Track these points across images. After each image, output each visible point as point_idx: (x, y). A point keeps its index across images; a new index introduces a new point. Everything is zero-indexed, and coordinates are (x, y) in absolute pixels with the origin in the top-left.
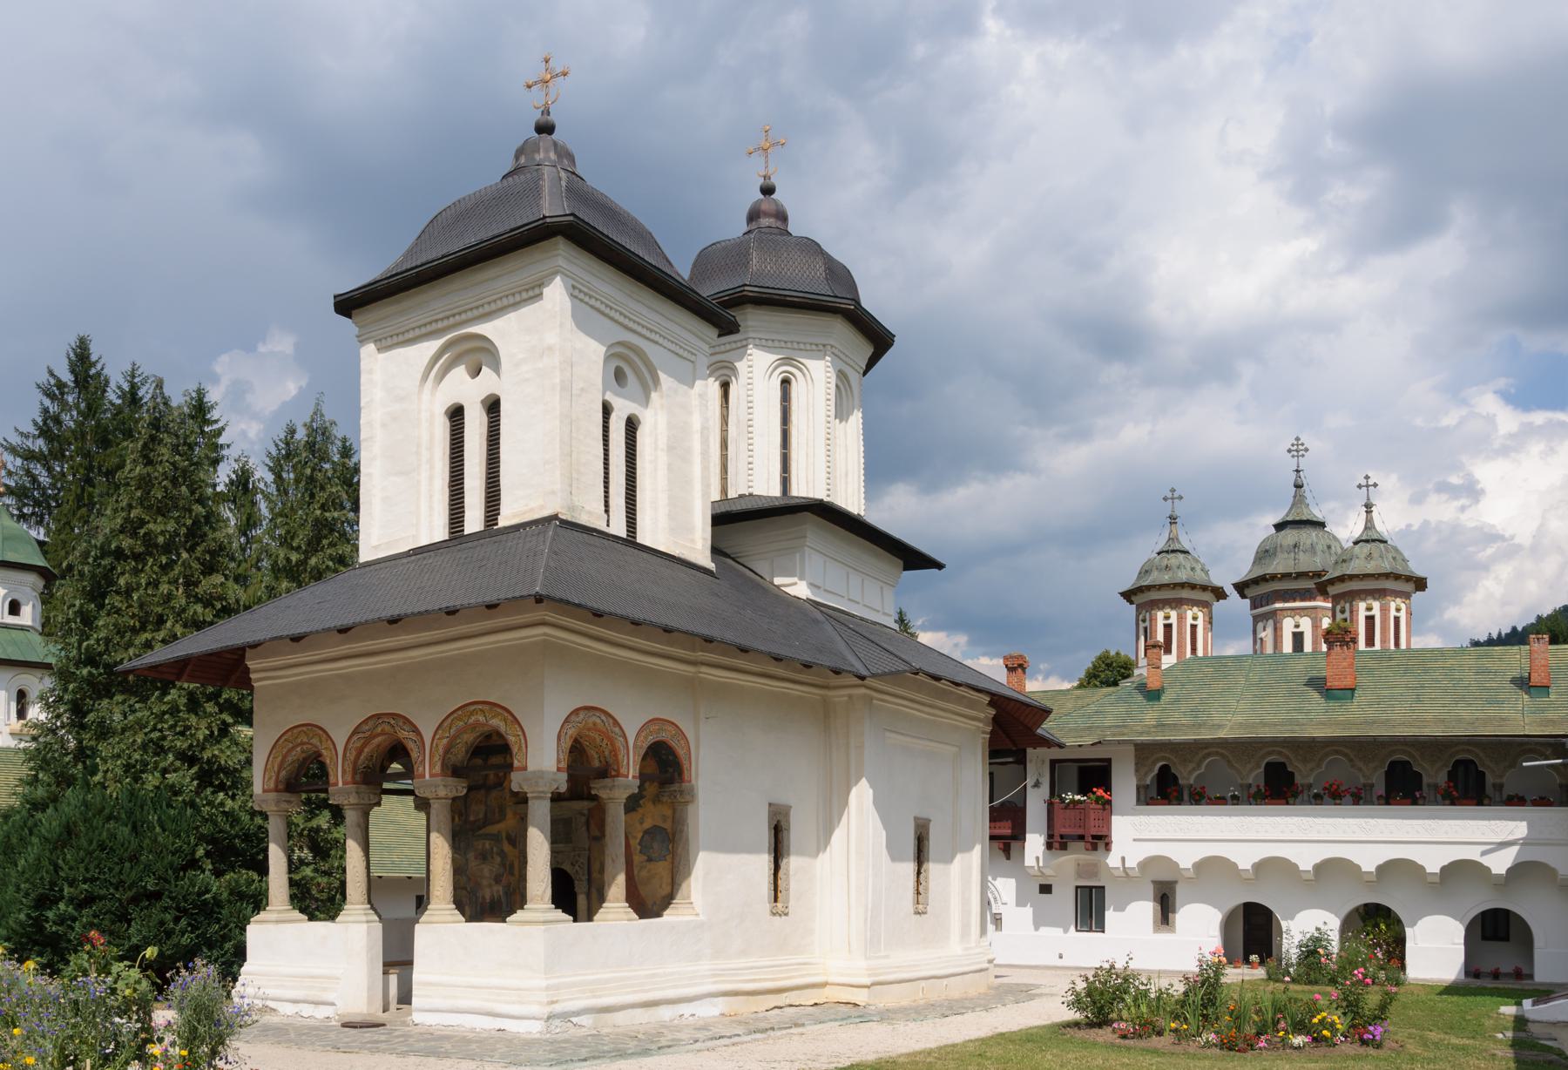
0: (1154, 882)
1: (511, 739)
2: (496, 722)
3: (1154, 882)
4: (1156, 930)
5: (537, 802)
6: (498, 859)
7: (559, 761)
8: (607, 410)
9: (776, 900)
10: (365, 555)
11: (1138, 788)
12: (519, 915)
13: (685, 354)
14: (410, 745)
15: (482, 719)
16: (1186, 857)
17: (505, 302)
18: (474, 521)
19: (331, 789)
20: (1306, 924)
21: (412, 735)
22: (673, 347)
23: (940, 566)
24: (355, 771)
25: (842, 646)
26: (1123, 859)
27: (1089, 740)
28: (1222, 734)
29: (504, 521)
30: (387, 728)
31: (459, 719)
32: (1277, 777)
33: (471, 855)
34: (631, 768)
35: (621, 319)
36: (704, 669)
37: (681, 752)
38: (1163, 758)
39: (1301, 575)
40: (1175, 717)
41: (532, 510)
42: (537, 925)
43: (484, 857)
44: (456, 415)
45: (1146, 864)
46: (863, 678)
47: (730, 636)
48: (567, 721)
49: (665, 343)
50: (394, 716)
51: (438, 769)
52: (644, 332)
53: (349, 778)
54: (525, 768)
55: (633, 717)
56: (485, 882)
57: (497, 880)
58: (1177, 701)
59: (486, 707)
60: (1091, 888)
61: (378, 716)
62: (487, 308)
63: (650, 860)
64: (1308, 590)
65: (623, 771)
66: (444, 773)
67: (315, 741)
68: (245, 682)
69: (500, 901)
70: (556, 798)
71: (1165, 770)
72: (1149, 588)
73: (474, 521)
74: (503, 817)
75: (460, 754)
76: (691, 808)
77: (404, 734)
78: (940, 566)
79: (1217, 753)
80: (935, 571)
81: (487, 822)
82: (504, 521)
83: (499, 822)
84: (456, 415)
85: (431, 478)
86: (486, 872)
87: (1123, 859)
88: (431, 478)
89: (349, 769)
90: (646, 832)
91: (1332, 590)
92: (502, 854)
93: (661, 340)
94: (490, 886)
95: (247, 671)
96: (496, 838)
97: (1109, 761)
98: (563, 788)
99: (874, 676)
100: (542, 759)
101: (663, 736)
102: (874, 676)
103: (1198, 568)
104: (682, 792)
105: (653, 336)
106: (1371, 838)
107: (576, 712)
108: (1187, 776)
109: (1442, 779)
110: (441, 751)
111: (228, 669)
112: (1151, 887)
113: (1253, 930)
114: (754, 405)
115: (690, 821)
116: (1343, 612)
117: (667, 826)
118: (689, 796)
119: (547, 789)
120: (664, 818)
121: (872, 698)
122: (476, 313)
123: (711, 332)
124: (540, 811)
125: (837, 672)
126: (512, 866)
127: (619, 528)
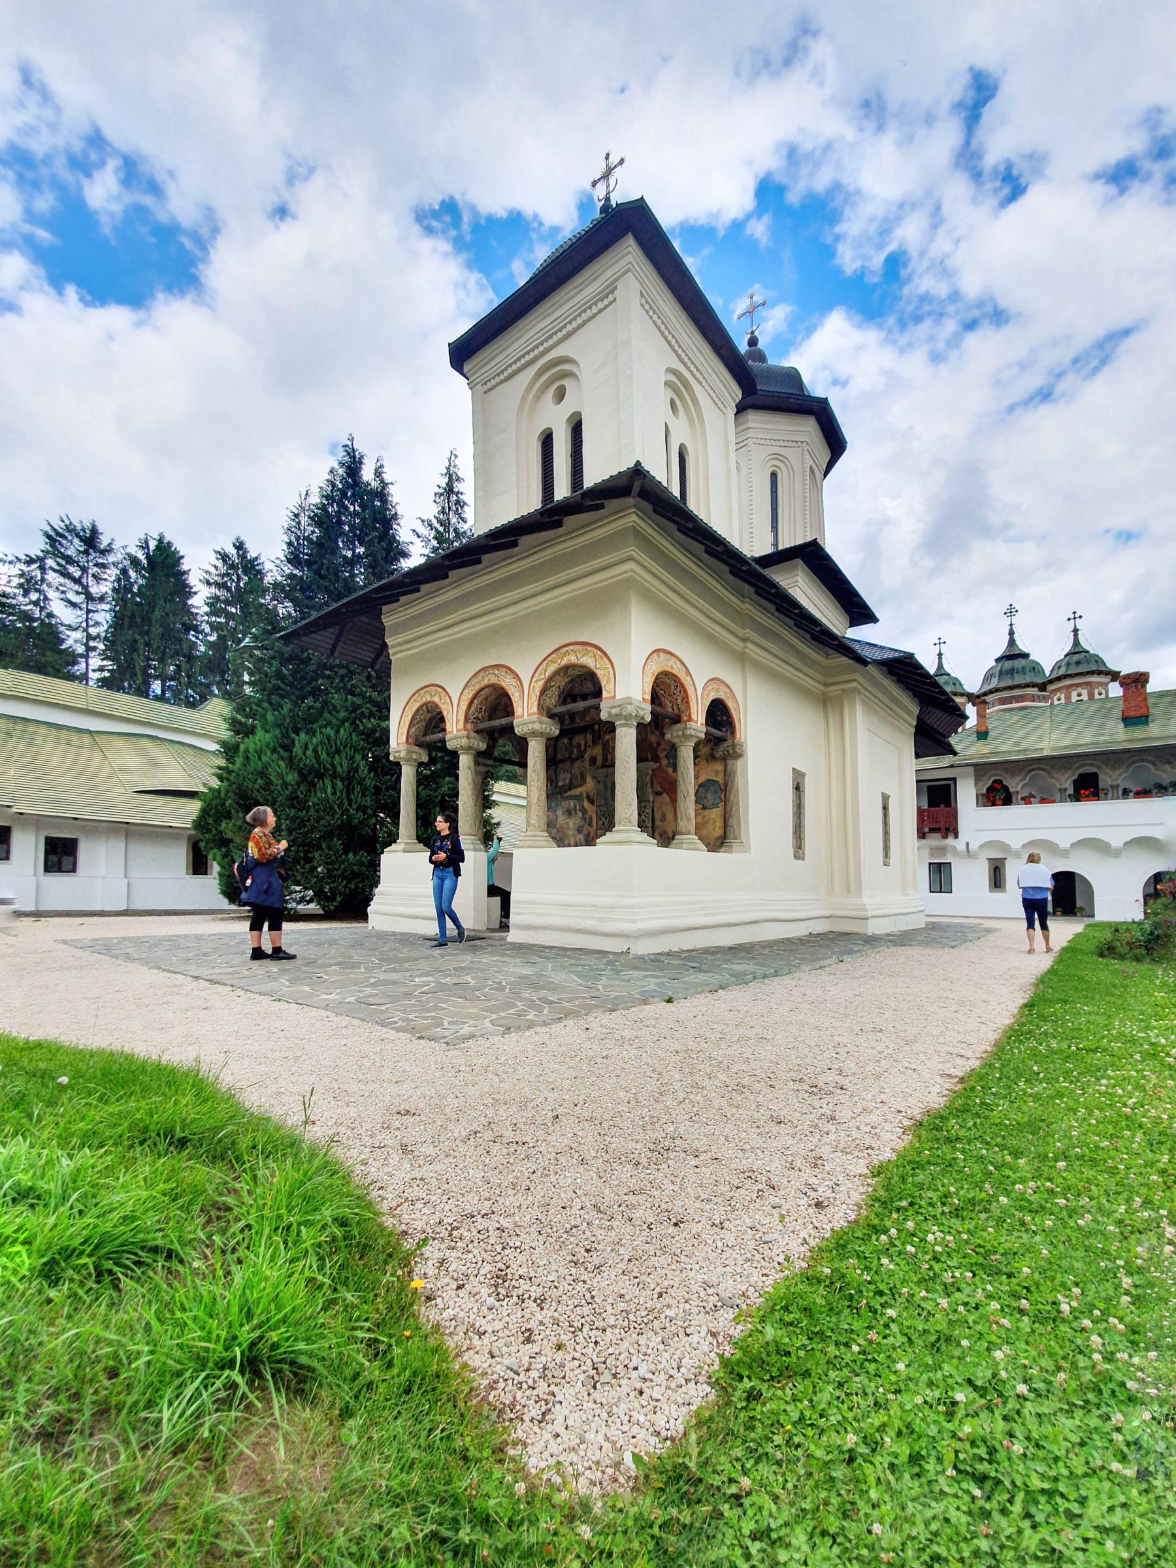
5: (624, 729)
6: (580, 814)
7: (644, 693)
12: (609, 836)
16: (1016, 841)
17: (584, 317)
21: (514, 682)
26: (967, 844)
28: (1045, 753)
29: (589, 482)
31: (553, 662)
33: (559, 813)
40: (1002, 747)
42: (626, 849)
44: (547, 441)
52: (692, 368)
56: (570, 833)
57: (579, 831)
59: (576, 647)
62: (569, 328)
63: (704, 808)
65: (694, 716)
67: (436, 699)
73: (562, 491)
74: (584, 782)
77: (507, 683)
81: (571, 786)
82: (589, 482)
84: (547, 441)
86: (571, 825)
87: (967, 844)
91: (1050, 688)
92: (584, 811)
96: (578, 798)
101: (721, 695)
120: (716, 772)
122: (560, 335)
124: (626, 743)
126: (591, 819)
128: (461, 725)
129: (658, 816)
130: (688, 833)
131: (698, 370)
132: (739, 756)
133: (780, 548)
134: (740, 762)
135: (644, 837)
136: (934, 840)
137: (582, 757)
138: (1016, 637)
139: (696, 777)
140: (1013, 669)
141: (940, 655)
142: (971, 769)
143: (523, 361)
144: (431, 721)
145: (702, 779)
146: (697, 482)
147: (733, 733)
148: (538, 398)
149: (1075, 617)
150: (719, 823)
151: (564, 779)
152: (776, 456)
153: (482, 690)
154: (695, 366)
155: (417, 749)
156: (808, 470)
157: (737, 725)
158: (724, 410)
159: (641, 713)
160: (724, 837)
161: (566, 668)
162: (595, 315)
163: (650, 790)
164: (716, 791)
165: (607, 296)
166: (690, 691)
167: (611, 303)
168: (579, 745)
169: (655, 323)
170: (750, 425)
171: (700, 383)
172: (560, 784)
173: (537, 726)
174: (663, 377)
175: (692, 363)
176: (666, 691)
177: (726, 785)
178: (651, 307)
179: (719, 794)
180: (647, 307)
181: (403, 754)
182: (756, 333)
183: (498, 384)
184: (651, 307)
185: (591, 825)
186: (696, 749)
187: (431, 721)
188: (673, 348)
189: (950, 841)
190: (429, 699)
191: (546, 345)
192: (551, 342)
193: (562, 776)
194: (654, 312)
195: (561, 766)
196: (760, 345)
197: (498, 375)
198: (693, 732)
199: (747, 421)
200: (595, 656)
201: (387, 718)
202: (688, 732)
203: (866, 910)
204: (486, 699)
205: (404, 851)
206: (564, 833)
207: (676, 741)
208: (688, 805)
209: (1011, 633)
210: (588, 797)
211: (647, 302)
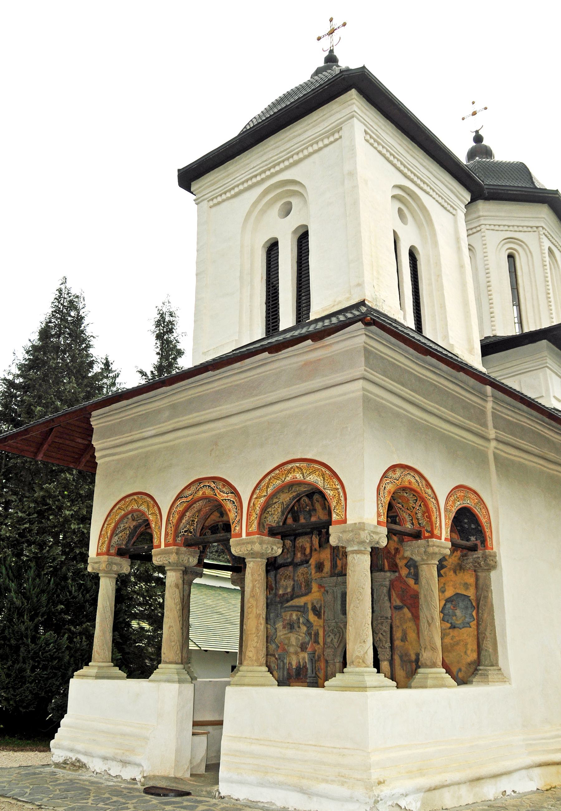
2: (312, 478)
6: (304, 629)
7: (379, 515)
13: (449, 208)
18: (287, 319)
21: (231, 497)
24: (176, 535)
29: (317, 310)
30: (208, 492)
33: (279, 625)
35: (402, 168)
37: (483, 520)
41: (340, 302)
43: (291, 626)
44: (272, 249)
48: (385, 475)
49: (434, 195)
50: (214, 479)
52: (419, 182)
53: (170, 539)
54: (345, 521)
55: (442, 481)
56: (292, 650)
57: (303, 647)
59: (304, 464)
61: (200, 481)
62: (296, 158)
63: (453, 627)
66: (260, 531)
67: (143, 508)
69: (305, 667)
73: (287, 319)
74: (308, 591)
75: (274, 518)
77: (223, 496)
83: (306, 594)
84: (272, 249)
85: (251, 296)
88: (251, 296)
89: (171, 531)
92: (308, 624)
93: (431, 192)
94: (296, 653)
96: (302, 609)
100: (361, 513)
101: (469, 503)
105: (425, 187)
107: (393, 468)
114: (491, 270)
115: (494, 587)
117: (471, 593)
118: (490, 564)
120: (466, 586)
124: (360, 568)
126: (317, 634)
129: (398, 635)
130: (434, 665)
131: (424, 183)
132: (494, 567)
133: (526, 330)
134: (493, 574)
137: (307, 562)
139: (442, 590)
143: (250, 183)
145: (449, 593)
147: (484, 541)
148: (263, 211)
150: (472, 645)
151: (285, 586)
154: (421, 180)
155: (118, 559)
156: (547, 251)
158: (454, 212)
159: (376, 537)
160: (479, 662)
161: (291, 485)
162: (320, 149)
163: (387, 604)
164: (467, 608)
165: (333, 134)
166: (432, 504)
167: (336, 140)
168: (303, 549)
169: (380, 152)
170: (481, 214)
171: (428, 193)
172: (281, 592)
173: (257, 547)
174: (392, 192)
175: (418, 177)
176: (403, 506)
177: (478, 601)
178: (375, 141)
179: (473, 610)
180: (372, 141)
181: (103, 566)
182: (480, 133)
183: (224, 201)
184: (375, 141)
185: (316, 642)
186: (440, 567)
188: (400, 171)
190: (135, 507)
191: (273, 170)
192: (277, 168)
193: (283, 583)
194: (379, 144)
195: (281, 571)
196: (485, 142)
197: (225, 193)
198: (436, 550)
199: (478, 210)
200: (323, 475)
202: (431, 550)
204: (199, 511)
205: (98, 677)
206: (284, 650)
207: (417, 558)
208: (434, 631)
210: (314, 609)
211: (371, 137)
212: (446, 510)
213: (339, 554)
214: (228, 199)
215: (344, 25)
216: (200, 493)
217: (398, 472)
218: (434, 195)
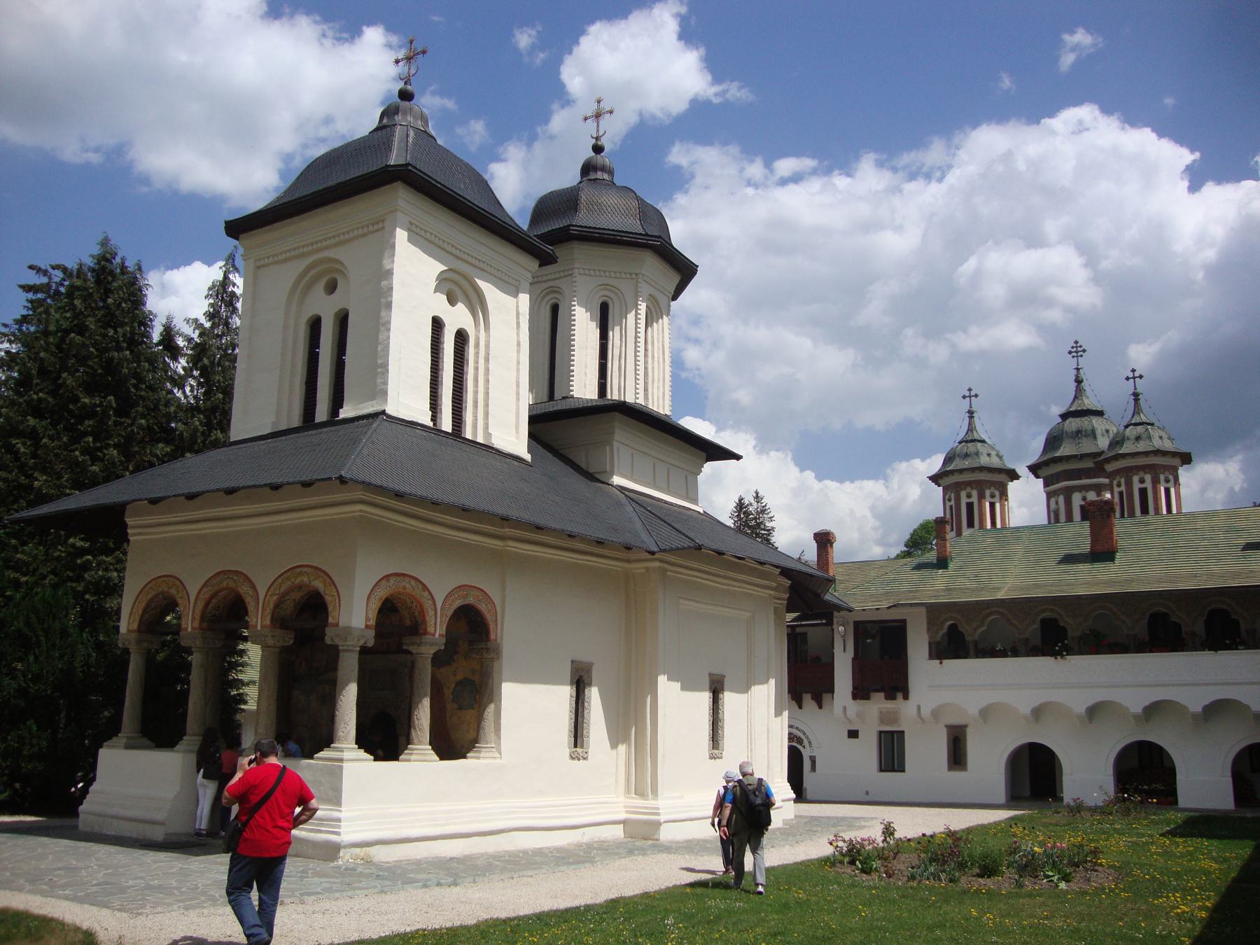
0: (947, 726)
1: (328, 598)
3: (947, 726)
4: (950, 768)
7: (367, 619)
8: (437, 325)
9: (576, 746)
10: (236, 433)
11: (930, 644)
14: (248, 600)
15: (306, 579)
19: (182, 633)
20: (1087, 774)
22: (499, 274)
23: (738, 457)
24: (203, 618)
25: (638, 525)
26: (919, 707)
27: (885, 604)
31: (288, 579)
32: (1052, 629)
34: (437, 628)
35: (454, 251)
36: (510, 543)
37: (489, 617)
38: (951, 618)
39: (1083, 457)
44: (315, 325)
45: (936, 713)
46: (653, 553)
47: (525, 516)
49: (493, 271)
50: (237, 572)
51: (268, 622)
54: (337, 625)
58: (961, 568)
60: (892, 733)
61: (224, 572)
63: (460, 708)
64: (1090, 469)
65: (431, 630)
67: (173, 591)
68: (122, 538)
70: (364, 651)
71: (953, 628)
72: (952, 472)
76: (496, 664)
77: (244, 590)
78: (738, 457)
79: (998, 612)
80: (733, 462)
82: (345, 413)
84: (315, 325)
87: (919, 707)
90: (459, 683)
91: (1110, 468)
95: (125, 526)
97: (904, 621)
98: (371, 644)
99: (661, 551)
100: (355, 615)
101: (471, 600)
102: (661, 551)
103: (993, 453)
104: (488, 649)
106: (1131, 682)
107: (387, 577)
108: (972, 632)
109: (1200, 627)
110: (272, 606)
111: (108, 528)
112: (944, 731)
113: (1035, 774)
116: (1119, 485)
119: (355, 644)
121: (666, 570)
123: (533, 264)
124: (349, 664)
125: (628, 548)
127: (447, 425)
128: (196, 624)
135: (362, 754)
136: (878, 704)
138: (1085, 385)
140: (1079, 432)
141: (971, 413)
142: (923, 610)
144: (161, 608)
146: (477, 362)
149: (970, 395)
152: (605, 286)
153: (220, 591)
157: (492, 627)
161: (300, 587)
187: (161, 608)
189: (899, 703)
201: (119, 620)
203: (658, 814)
209: (1079, 381)
212: (442, 615)
213: (333, 654)
214: (276, 263)
215: (424, 52)
216: (225, 584)
217: (392, 580)
218: (493, 271)
